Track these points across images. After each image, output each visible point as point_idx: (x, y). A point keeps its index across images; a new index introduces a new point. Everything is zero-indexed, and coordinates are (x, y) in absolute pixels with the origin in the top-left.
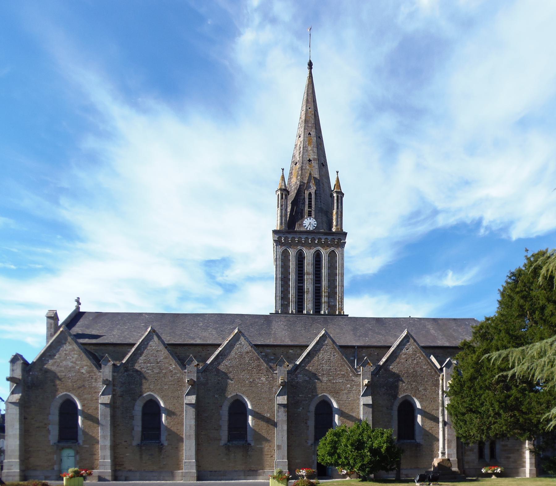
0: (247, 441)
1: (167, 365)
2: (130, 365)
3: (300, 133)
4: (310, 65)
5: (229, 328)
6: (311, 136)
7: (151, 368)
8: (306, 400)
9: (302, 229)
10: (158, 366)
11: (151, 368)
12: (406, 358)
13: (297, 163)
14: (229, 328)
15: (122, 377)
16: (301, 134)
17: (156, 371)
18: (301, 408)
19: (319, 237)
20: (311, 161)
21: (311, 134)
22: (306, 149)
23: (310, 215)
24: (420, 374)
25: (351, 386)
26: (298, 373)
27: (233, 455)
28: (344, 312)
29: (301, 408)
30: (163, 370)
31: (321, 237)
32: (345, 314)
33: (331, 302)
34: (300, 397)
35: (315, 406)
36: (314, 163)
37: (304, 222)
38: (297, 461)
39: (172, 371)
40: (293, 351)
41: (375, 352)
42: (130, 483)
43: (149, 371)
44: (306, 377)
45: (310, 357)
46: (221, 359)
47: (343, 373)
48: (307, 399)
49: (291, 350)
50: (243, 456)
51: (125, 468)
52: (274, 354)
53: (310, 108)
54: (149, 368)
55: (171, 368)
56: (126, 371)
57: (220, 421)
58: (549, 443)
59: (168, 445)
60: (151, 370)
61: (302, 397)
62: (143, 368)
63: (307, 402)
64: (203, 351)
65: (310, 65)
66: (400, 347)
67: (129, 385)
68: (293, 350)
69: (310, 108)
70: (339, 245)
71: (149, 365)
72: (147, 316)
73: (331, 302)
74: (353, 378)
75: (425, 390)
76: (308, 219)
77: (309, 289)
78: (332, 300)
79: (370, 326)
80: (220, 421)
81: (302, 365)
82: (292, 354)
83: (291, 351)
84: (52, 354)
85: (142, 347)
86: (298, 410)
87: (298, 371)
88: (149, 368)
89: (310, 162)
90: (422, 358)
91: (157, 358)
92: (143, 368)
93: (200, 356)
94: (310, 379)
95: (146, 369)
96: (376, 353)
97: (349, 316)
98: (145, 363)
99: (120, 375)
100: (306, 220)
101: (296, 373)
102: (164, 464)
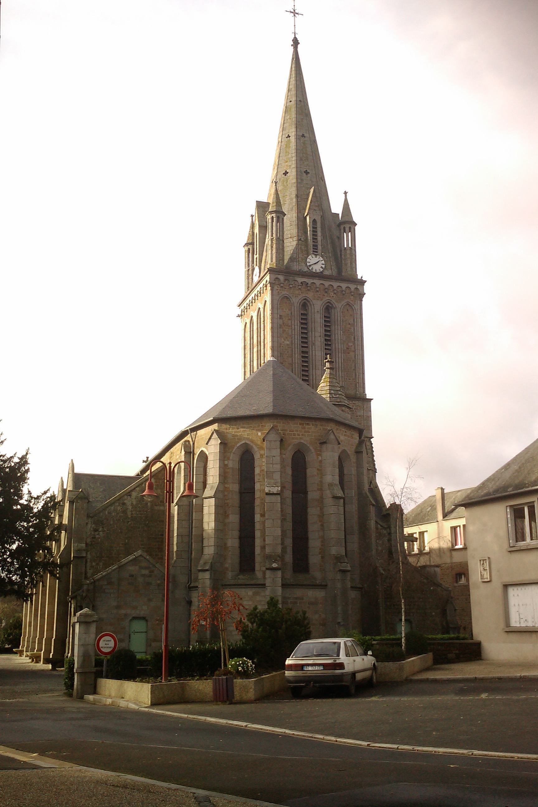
4: (296, 43)
23: (315, 253)
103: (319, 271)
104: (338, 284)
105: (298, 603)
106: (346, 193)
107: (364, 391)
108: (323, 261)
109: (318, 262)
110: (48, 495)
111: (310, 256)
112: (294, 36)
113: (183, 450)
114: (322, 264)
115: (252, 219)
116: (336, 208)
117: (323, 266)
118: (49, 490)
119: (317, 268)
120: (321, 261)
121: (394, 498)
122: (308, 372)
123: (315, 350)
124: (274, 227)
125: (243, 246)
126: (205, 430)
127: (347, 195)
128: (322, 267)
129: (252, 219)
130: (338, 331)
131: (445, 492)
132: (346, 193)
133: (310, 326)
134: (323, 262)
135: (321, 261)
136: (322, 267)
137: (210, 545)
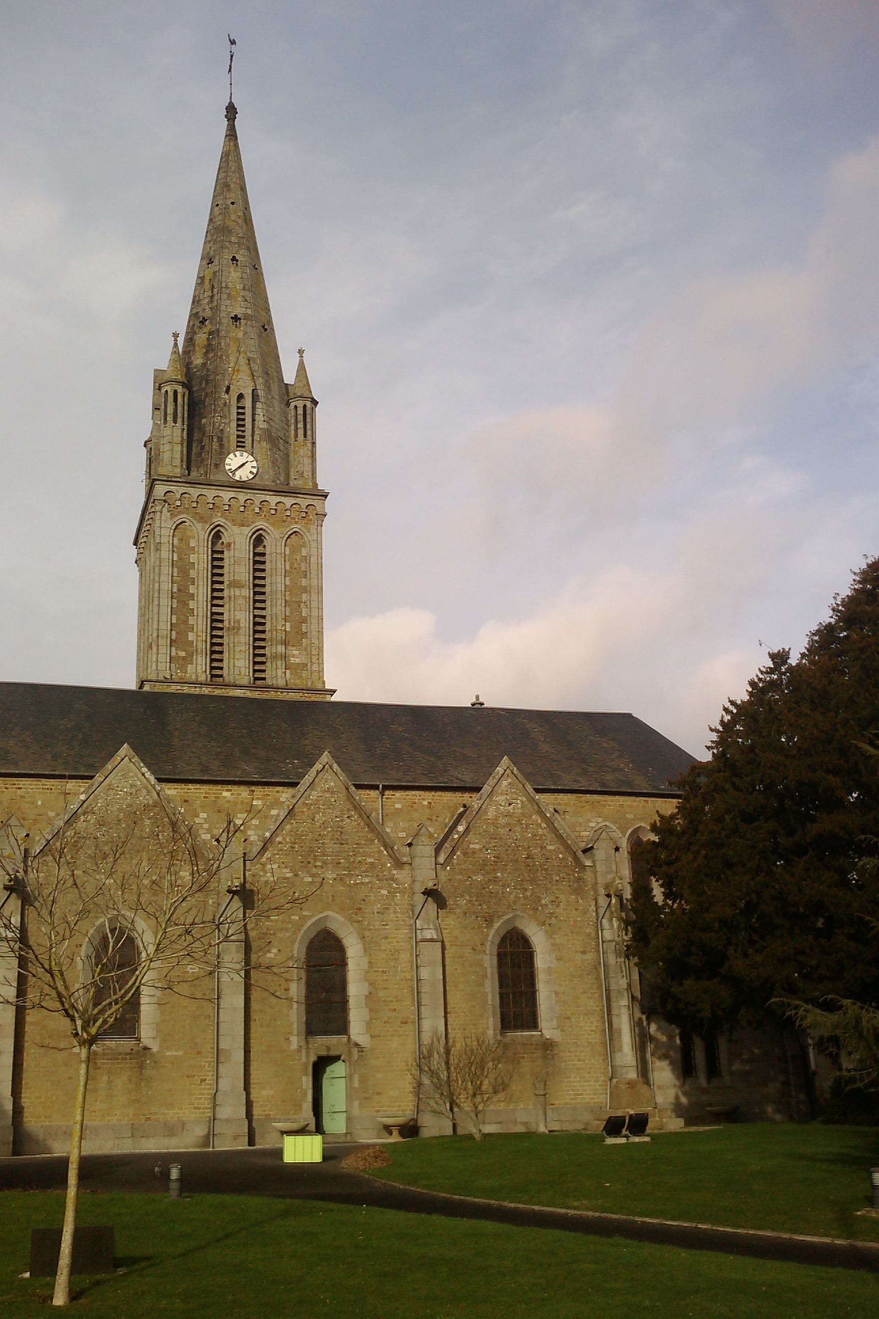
4: (231, 112)
6: (237, 265)
8: (287, 929)
9: (220, 477)
12: (508, 824)
18: (275, 950)
20: (240, 319)
21: (237, 261)
22: (228, 291)
23: (240, 446)
24: (541, 865)
27: (105, 1078)
28: (324, 683)
29: (275, 950)
31: (268, 498)
33: (294, 656)
34: (272, 921)
36: (246, 324)
37: (227, 461)
38: (271, 1093)
42: (773, 1230)
44: (285, 870)
46: (84, 821)
48: (290, 926)
49: (227, 791)
50: (130, 1080)
52: (185, 801)
53: (233, 203)
58: (489, 814)
61: (277, 920)
63: (287, 935)
64: (6, 788)
65: (231, 112)
66: (494, 799)
68: (230, 790)
69: (233, 203)
70: (311, 520)
73: (294, 656)
74: (395, 872)
75: (556, 902)
76: (237, 453)
78: (294, 652)
79: (400, 729)
81: (277, 839)
82: (229, 801)
83: (225, 794)
86: (268, 955)
87: (268, 854)
90: (544, 825)
94: (296, 875)
96: (425, 803)
100: (231, 456)
104: (279, 499)
105: (174, 1186)
106: (301, 352)
107: (321, 671)
108: (255, 462)
109: (243, 464)
111: (232, 454)
112: (229, 101)
114: (252, 467)
117: (255, 471)
119: (244, 475)
122: (265, 618)
123: (170, 662)
124: (169, 405)
128: (251, 472)
131: (132, 686)
132: (301, 352)
136: (251, 472)
137: (160, 647)
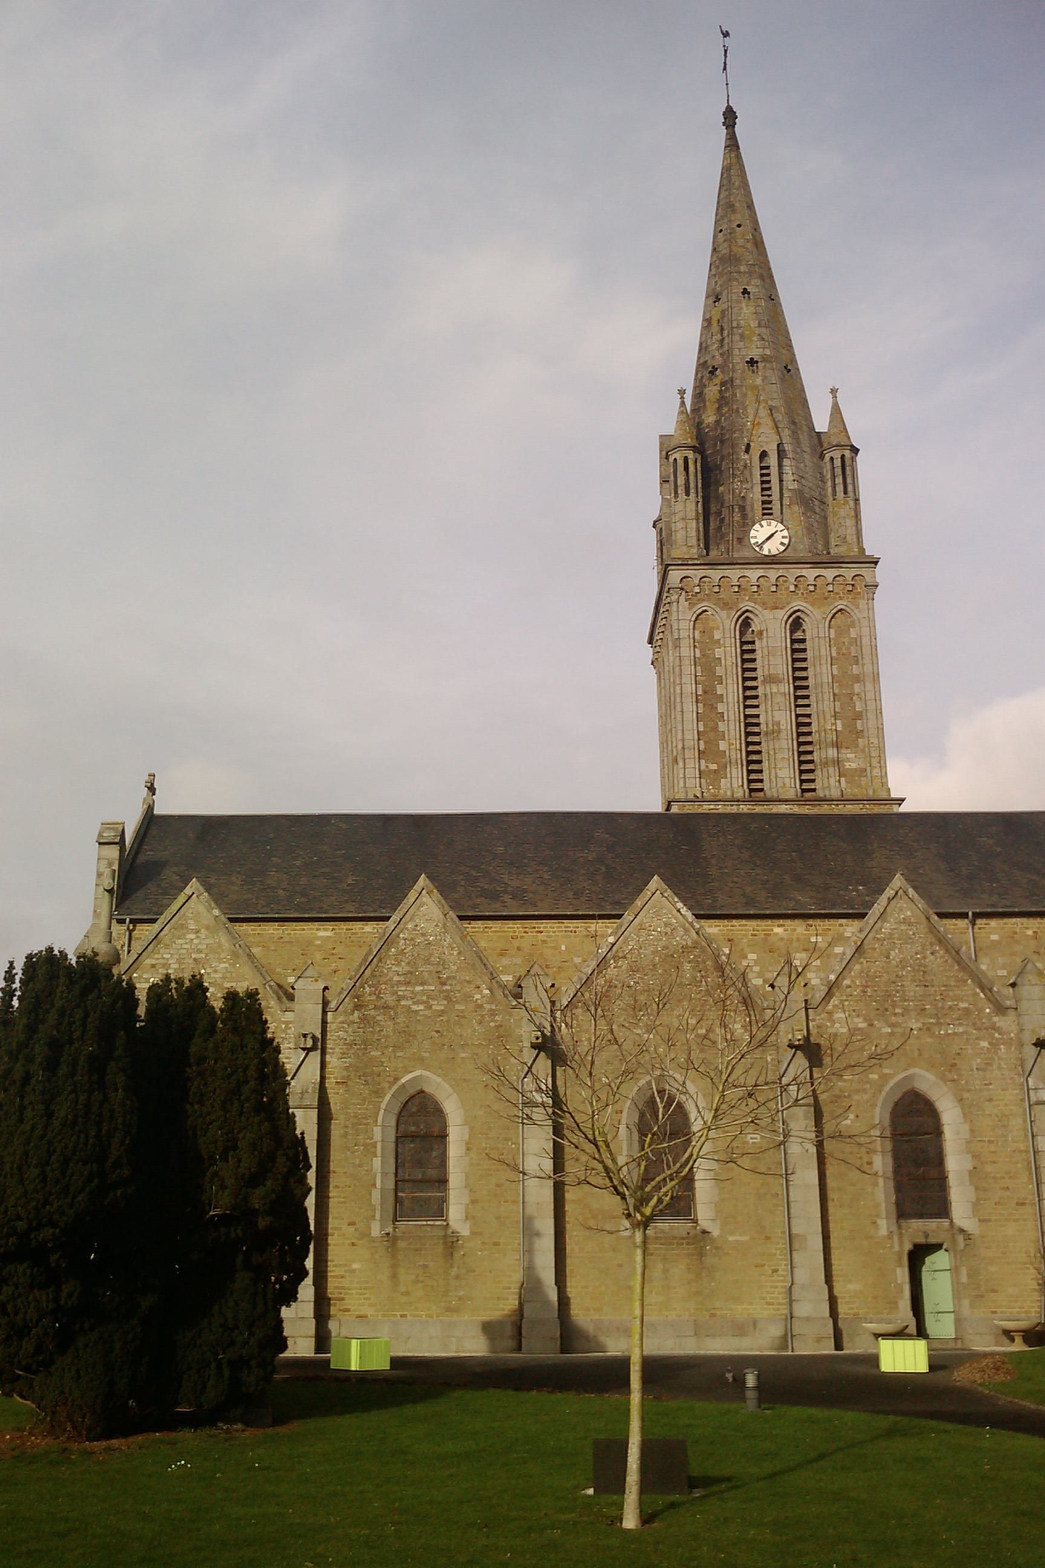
0: (695, 1221)
1: (468, 989)
2: (367, 989)
3: (718, 289)
4: (730, 117)
5: (581, 860)
6: (749, 298)
7: (425, 998)
8: (864, 1091)
9: (746, 553)
10: (443, 991)
11: (425, 998)
13: (715, 369)
14: (581, 860)
15: (346, 1026)
16: (721, 293)
17: (438, 1006)
18: (852, 1116)
19: (798, 573)
20: (757, 362)
21: (749, 293)
22: (740, 331)
23: (767, 513)
25: (990, 1043)
26: (835, 1006)
30: (457, 1002)
32: (893, 796)
33: (849, 760)
34: (845, 1081)
35: (890, 1110)
36: (764, 368)
37: (753, 533)
39: (481, 1006)
40: (786, 930)
41: (1027, 928)
43: (421, 1007)
44: (856, 1020)
45: (865, 958)
47: (965, 1005)
48: (868, 1086)
49: (779, 926)
51: (348, 1310)
53: (739, 226)
54: (419, 997)
55: (478, 996)
56: (357, 1007)
57: (974, 1200)
59: (473, 1233)
60: (423, 1002)
62: (404, 997)
64: (526, 932)
67: (365, 1049)
69: (739, 226)
71: (419, 988)
72: (344, 826)
73: (849, 760)
74: (996, 1019)
76: (764, 523)
77: (778, 724)
78: (849, 756)
80: (974, 1200)
82: (782, 939)
83: (777, 930)
84: (161, 961)
85: (401, 936)
87: (834, 1001)
88: (419, 997)
89: (752, 366)
91: (440, 968)
92: (404, 997)
93: (519, 949)
94: (871, 1025)
95: (410, 1002)
96: (1030, 932)
97: (904, 808)
98: (408, 983)
99: (341, 1019)
100: (757, 526)
101: (830, 1007)
102: (460, 1299)
103: (777, 552)
106: (834, 391)
110: (18, 970)
113: (306, 1123)
114: (783, 537)
115: (682, 398)
116: (821, 423)
117: (786, 541)
118: (11, 963)
119: (773, 547)
120: (781, 531)
121: (986, 1029)
125: (104, 822)
126: (333, 1218)
127: (838, 395)
128: (782, 544)
129: (682, 398)
130: (821, 668)
132: (834, 391)
133: (701, 524)
134: (786, 533)
135: (781, 531)
136: (782, 544)
